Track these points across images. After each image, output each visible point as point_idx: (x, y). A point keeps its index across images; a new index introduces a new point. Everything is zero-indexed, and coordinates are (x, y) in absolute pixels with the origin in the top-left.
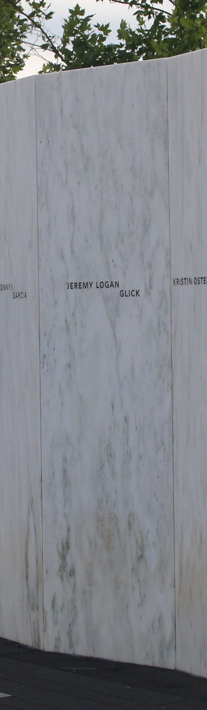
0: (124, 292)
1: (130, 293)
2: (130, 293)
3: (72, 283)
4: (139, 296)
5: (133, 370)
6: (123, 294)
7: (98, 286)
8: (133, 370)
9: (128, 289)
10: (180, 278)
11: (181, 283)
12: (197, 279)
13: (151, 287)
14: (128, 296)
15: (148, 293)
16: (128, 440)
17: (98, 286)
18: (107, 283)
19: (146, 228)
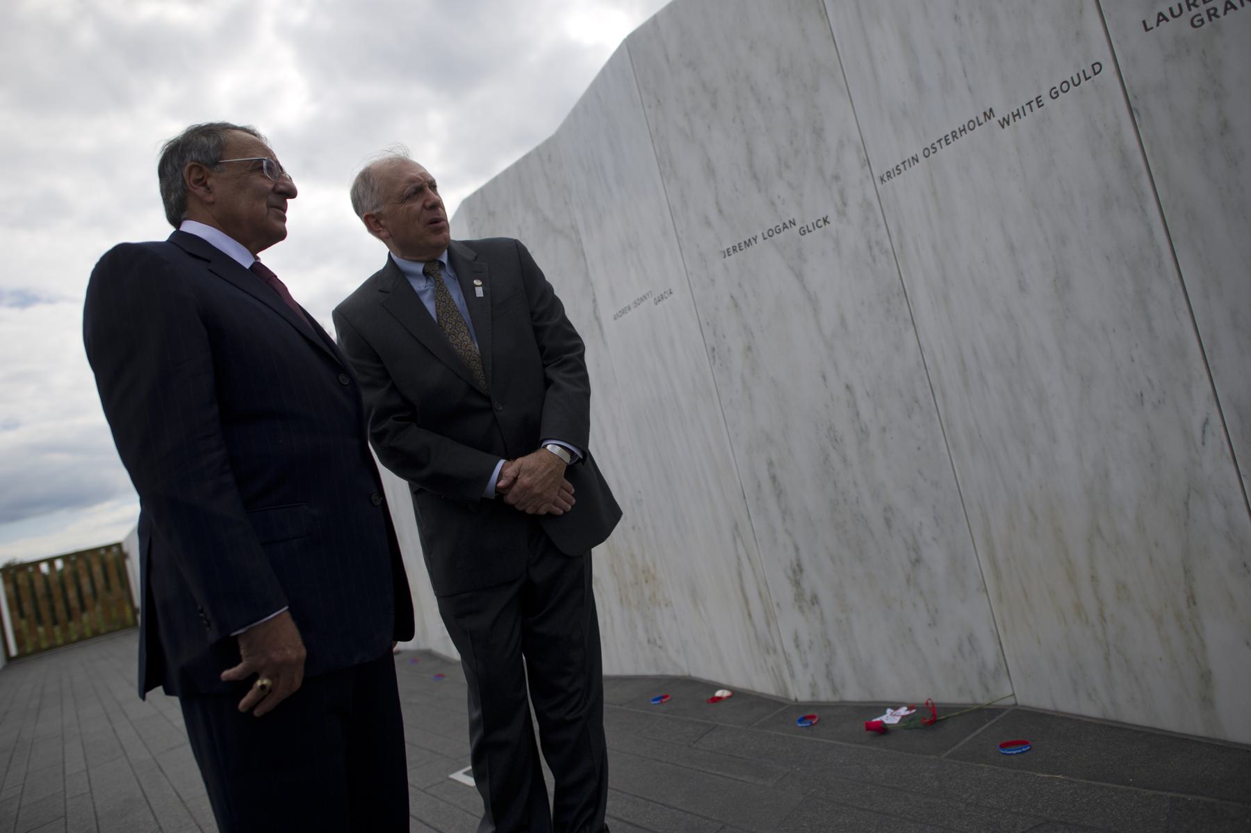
0: (806, 229)
1: (815, 225)
2: (815, 225)
3: (947, 136)
4: (999, 121)
5: (843, 321)
6: (803, 232)
7: (766, 236)
8: (843, 321)
9: (809, 222)
10: (891, 167)
11: (896, 172)
12: (929, 148)
13: (845, 204)
14: (813, 229)
15: (841, 213)
16: (858, 414)
17: (766, 236)
18: (1054, 91)
19: (818, 133)
